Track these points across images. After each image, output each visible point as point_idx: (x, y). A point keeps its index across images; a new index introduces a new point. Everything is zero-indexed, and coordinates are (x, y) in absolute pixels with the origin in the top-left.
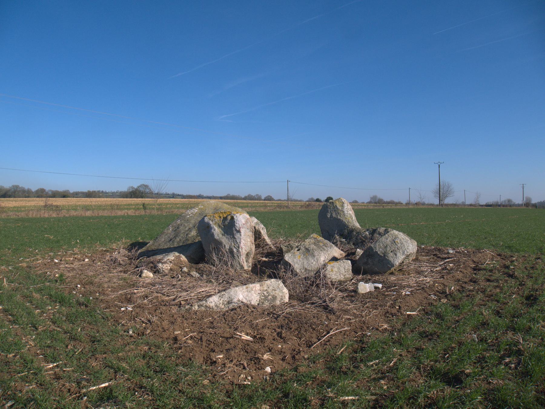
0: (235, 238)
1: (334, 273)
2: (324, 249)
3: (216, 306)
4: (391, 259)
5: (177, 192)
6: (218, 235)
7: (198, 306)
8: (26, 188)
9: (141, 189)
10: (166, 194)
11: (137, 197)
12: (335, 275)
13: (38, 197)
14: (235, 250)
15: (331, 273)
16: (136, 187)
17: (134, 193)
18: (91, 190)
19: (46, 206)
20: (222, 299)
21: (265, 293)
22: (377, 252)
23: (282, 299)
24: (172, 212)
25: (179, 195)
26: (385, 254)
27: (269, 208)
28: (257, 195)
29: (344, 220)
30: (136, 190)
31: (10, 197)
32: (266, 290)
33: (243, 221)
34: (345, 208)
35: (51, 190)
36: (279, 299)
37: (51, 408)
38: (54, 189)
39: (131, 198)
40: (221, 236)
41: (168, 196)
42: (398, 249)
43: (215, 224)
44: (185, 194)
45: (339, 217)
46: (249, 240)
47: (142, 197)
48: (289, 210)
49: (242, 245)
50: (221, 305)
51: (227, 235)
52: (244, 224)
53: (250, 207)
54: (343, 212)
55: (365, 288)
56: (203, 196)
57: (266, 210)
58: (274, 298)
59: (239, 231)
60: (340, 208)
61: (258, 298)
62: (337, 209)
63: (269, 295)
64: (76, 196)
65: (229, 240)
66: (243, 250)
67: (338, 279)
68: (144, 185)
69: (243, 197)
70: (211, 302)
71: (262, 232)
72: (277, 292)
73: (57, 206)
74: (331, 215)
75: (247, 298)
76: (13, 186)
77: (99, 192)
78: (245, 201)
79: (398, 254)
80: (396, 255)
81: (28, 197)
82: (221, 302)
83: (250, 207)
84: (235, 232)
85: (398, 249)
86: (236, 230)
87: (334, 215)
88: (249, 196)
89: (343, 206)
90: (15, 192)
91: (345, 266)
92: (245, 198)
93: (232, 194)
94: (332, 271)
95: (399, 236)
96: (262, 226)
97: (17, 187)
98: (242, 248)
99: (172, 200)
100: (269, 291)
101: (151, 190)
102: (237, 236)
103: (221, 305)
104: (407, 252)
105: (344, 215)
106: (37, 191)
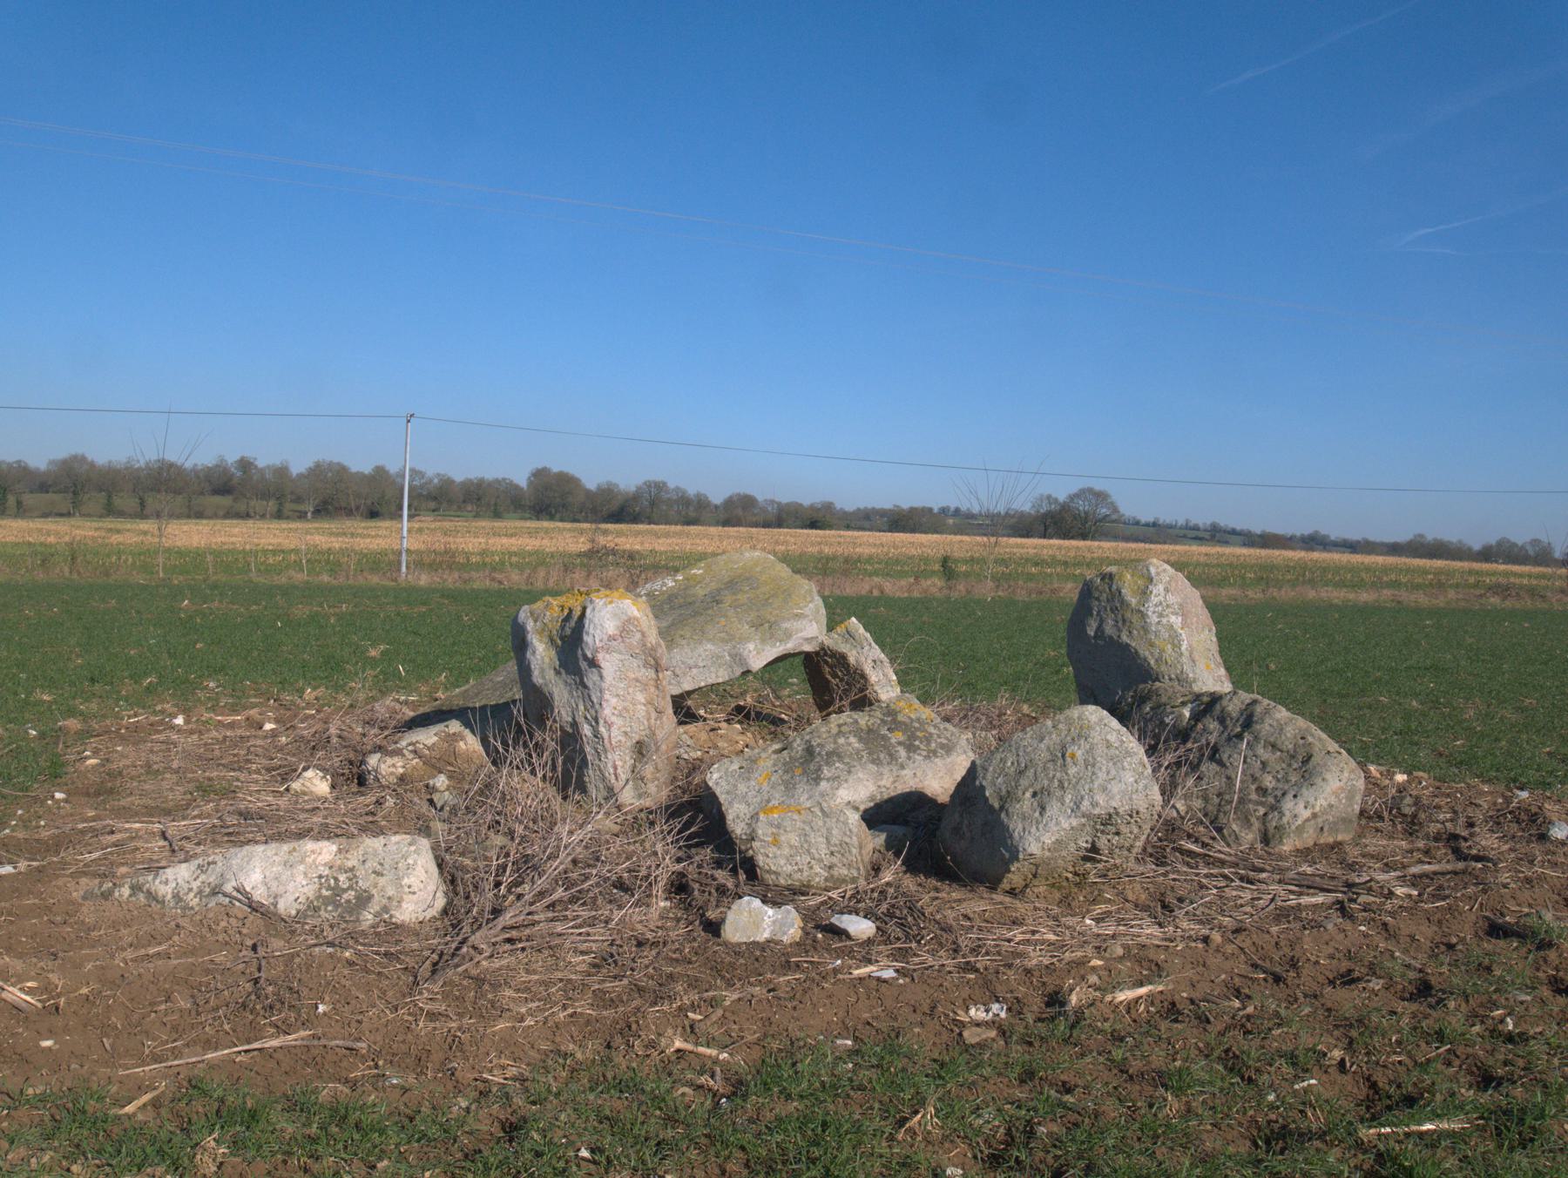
0: (585, 687)
1: (786, 851)
2: (893, 757)
3: (176, 896)
4: (1016, 826)
5: (1227, 521)
6: (542, 670)
7: (132, 888)
8: (691, 490)
9: (1082, 506)
10: (1187, 527)
11: (1066, 535)
12: (789, 859)
13: (727, 523)
14: (586, 730)
15: (772, 850)
16: (1062, 497)
17: (1058, 521)
18: (905, 505)
19: (590, 554)
20: (203, 877)
21: (342, 878)
22: (983, 788)
23: (385, 909)
24: (1053, 591)
25: (1234, 532)
26: (1007, 798)
27: (1451, 594)
28: (1535, 542)
29: (1144, 652)
30: (1065, 508)
31: (635, 519)
32: (352, 869)
33: (611, 627)
34: (1154, 600)
35: (772, 502)
36: (375, 906)
37: (867, 1175)
38: (784, 498)
39: (1044, 536)
40: (550, 674)
41: (1195, 533)
42: (1061, 786)
43: (540, 632)
44: (1257, 528)
45: (1125, 638)
46: (641, 697)
47: (1084, 537)
48: (1540, 604)
49: (607, 712)
50: (191, 895)
51: (568, 673)
52: (612, 638)
53: (1373, 585)
54: (1143, 616)
55: (758, 926)
56: (1325, 537)
57: (1440, 602)
58: (364, 899)
59: (593, 663)
60: (1133, 601)
61: (310, 891)
62: (1123, 602)
63: (350, 888)
64: (867, 524)
65: (570, 692)
66: (615, 732)
67: (797, 876)
68: (1090, 490)
69: (1477, 547)
70: (166, 883)
71: (873, 677)
72: (382, 881)
73: (631, 556)
74: (1100, 629)
75: (274, 885)
76: (648, 484)
77: (944, 510)
78: (1486, 566)
79: (1053, 809)
80: (1043, 808)
81: (689, 522)
82: (195, 885)
83: (1373, 585)
84: (583, 665)
85: (1061, 786)
86: (585, 657)
87: (1109, 629)
88: (1499, 544)
89: (1144, 594)
90: (653, 504)
91: (829, 830)
92: (1486, 555)
93: (1431, 535)
94: (776, 842)
95: (1096, 736)
96: (877, 652)
97: (660, 486)
98: (609, 726)
99: (321, 536)
100: (360, 873)
101: (1116, 510)
102: (591, 678)
103: (191, 895)
104: (1094, 805)
105: (1145, 629)
106: (729, 503)
